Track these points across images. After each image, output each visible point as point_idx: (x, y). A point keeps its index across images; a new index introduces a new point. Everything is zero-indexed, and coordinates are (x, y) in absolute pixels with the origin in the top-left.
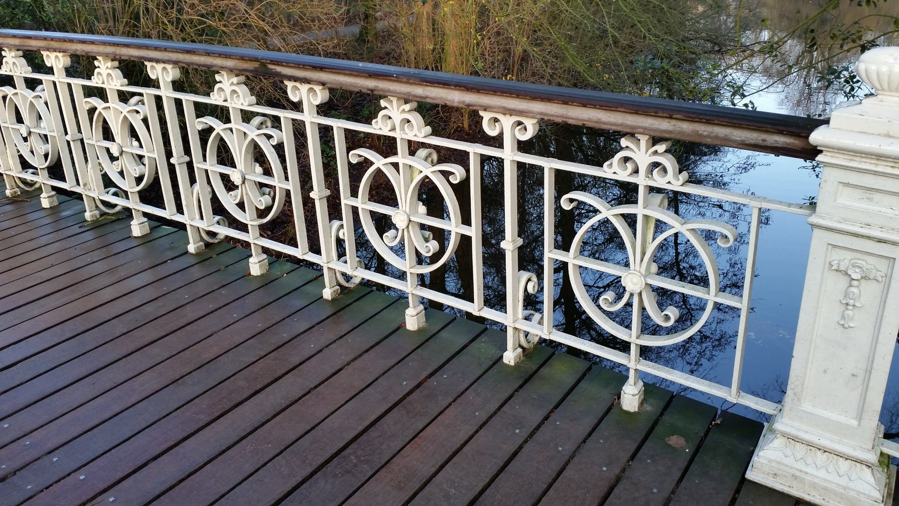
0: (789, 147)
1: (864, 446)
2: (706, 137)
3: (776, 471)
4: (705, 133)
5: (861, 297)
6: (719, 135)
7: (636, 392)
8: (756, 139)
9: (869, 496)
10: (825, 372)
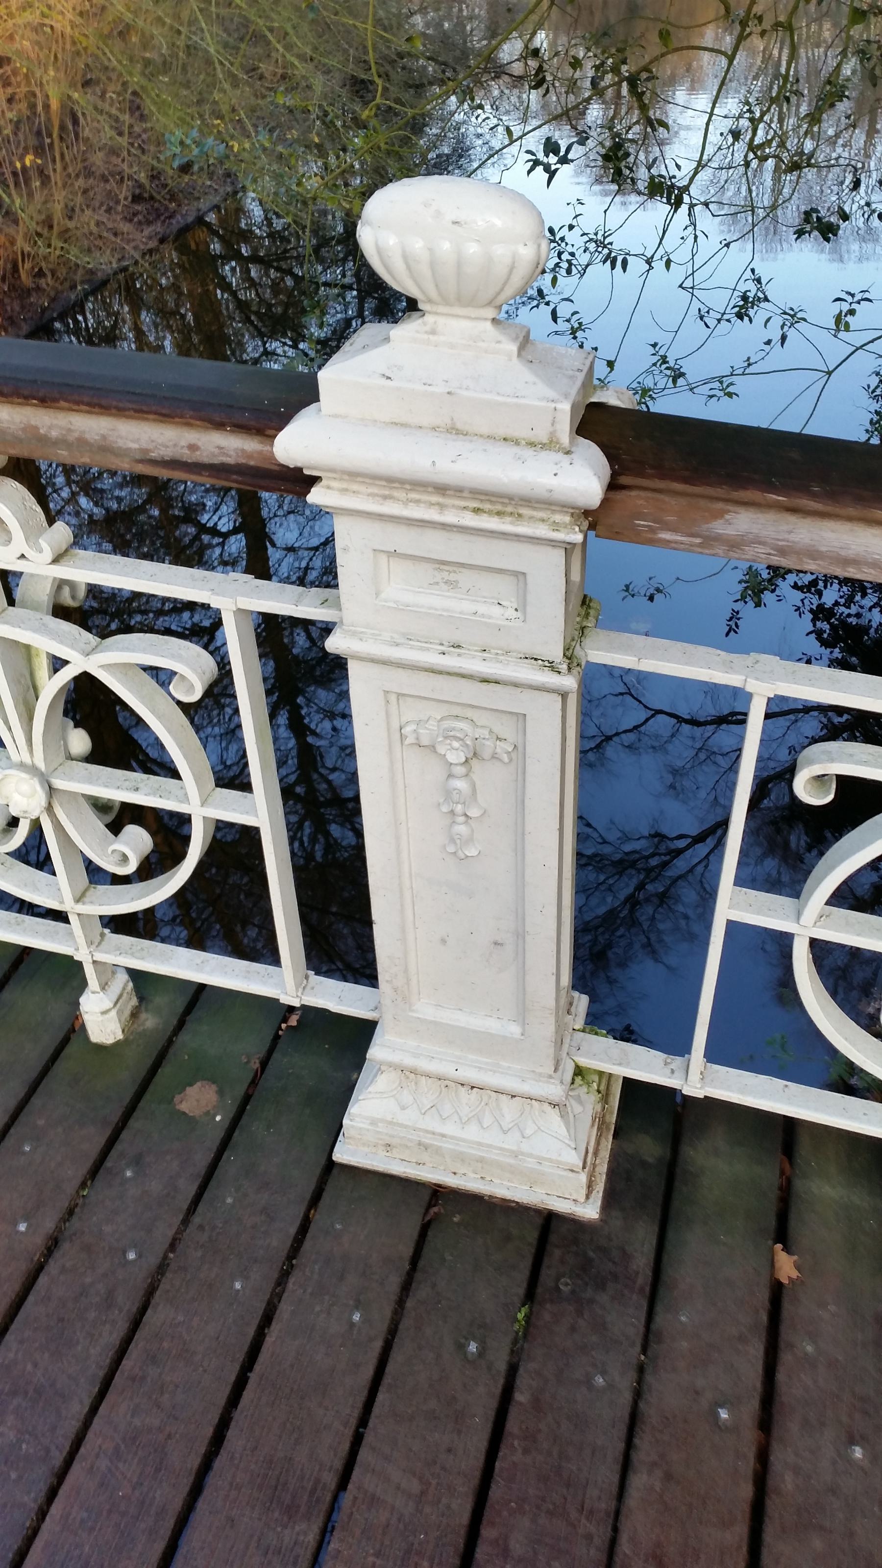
0: (252, 463)
1: (540, 1070)
2: (56, 443)
3: (388, 1140)
4: (54, 434)
5: (479, 796)
6: (87, 436)
7: (108, 1004)
8: (175, 445)
9: (558, 1164)
10: (444, 941)
